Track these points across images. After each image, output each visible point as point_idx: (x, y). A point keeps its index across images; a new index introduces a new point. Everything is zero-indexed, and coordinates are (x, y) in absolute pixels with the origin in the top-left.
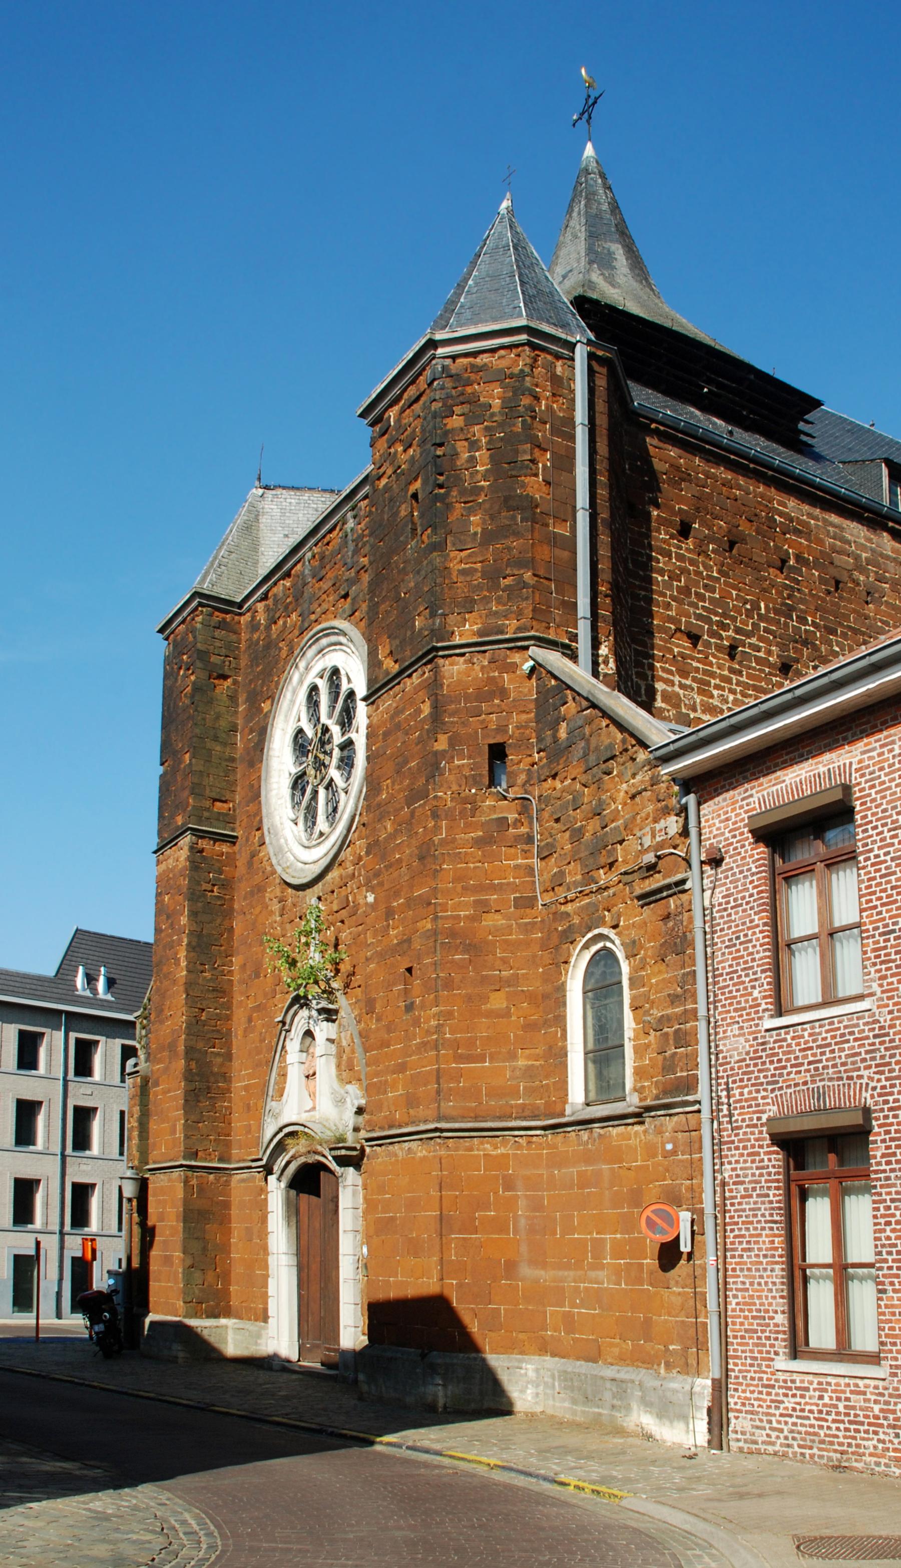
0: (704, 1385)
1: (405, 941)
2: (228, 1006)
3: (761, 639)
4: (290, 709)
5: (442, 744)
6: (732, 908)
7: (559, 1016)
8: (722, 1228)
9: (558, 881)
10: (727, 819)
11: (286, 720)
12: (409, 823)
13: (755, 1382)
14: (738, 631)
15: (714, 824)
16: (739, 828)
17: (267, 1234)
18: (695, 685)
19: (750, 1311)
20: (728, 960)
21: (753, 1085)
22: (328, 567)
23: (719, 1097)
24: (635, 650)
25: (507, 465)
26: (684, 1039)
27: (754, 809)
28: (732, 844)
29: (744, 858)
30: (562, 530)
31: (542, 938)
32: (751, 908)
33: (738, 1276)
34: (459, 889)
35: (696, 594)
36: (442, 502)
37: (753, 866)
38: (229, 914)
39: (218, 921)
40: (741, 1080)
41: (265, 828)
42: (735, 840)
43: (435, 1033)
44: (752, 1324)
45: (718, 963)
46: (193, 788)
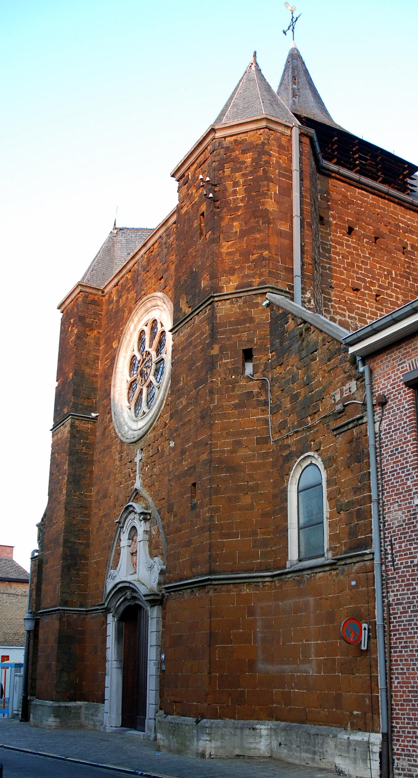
0: (376, 738)
1: (192, 467)
2: (89, 516)
3: (393, 291)
4: (128, 345)
5: (215, 351)
6: (393, 432)
7: (284, 507)
8: (387, 634)
9: (283, 425)
10: (389, 378)
11: (126, 352)
12: (196, 398)
13: (411, 735)
14: (380, 286)
15: (381, 382)
16: (397, 382)
17: (106, 649)
18: (357, 317)
19: (407, 687)
20: (390, 463)
21: (407, 541)
22: (152, 265)
23: (386, 550)
24: (324, 297)
25: (255, 190)
26: (365, 515)
27: (407, 370)
28: (392, 392)
29: (401, 400)
30: (284, 228)
31: (273, 461)
32: (405, 431)
33: (399, 665)
34: (224, 435)
35: (357, 266)
36: (218, 215)
37: (406, 405)
38: (91, 463)
39: (85, 467)
40: (400, 538)
41: (113, 413)
42: (394, 390)
43: (209, 521)
44: (409, 696)
45: (384, 466)
46: (74, 392)
